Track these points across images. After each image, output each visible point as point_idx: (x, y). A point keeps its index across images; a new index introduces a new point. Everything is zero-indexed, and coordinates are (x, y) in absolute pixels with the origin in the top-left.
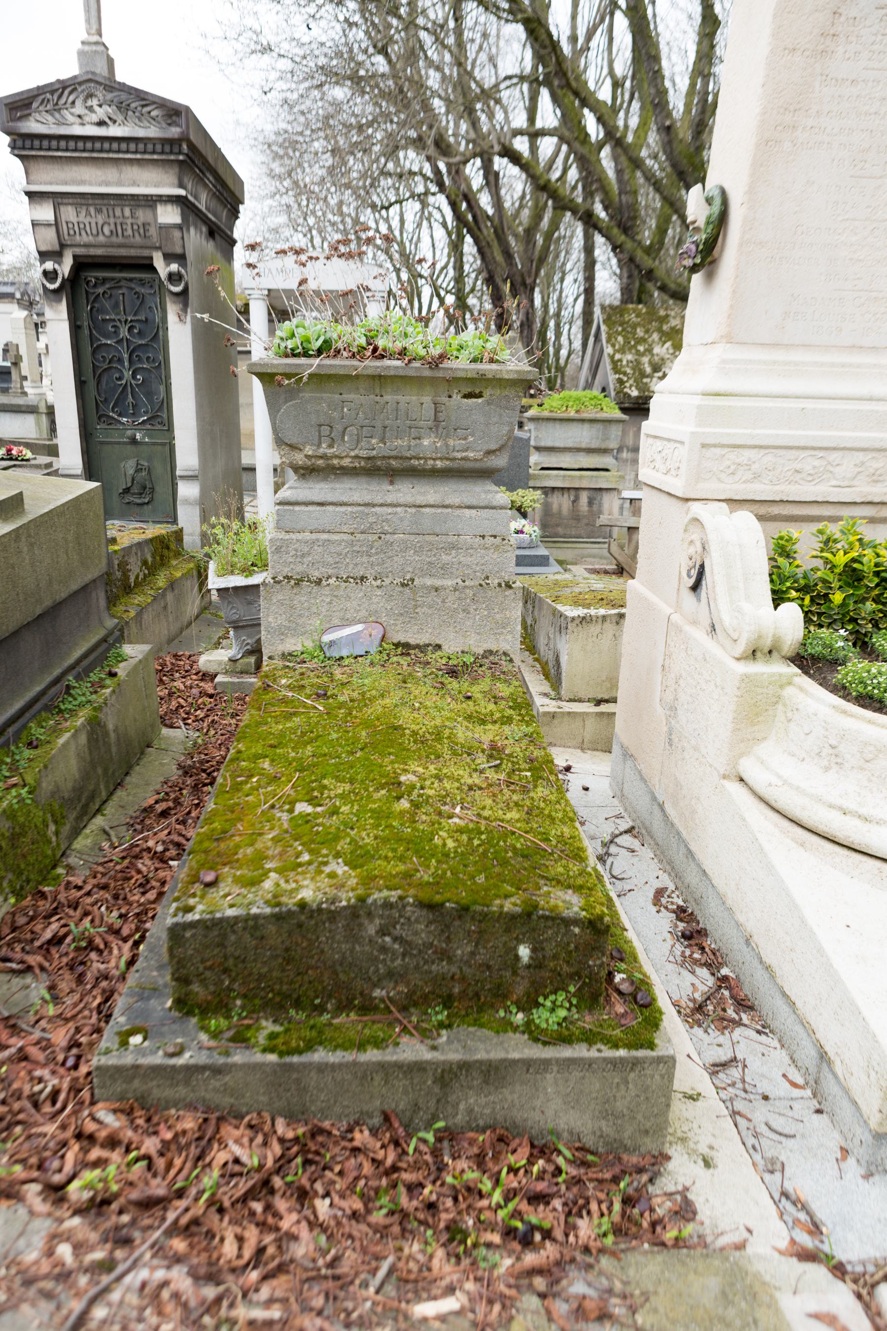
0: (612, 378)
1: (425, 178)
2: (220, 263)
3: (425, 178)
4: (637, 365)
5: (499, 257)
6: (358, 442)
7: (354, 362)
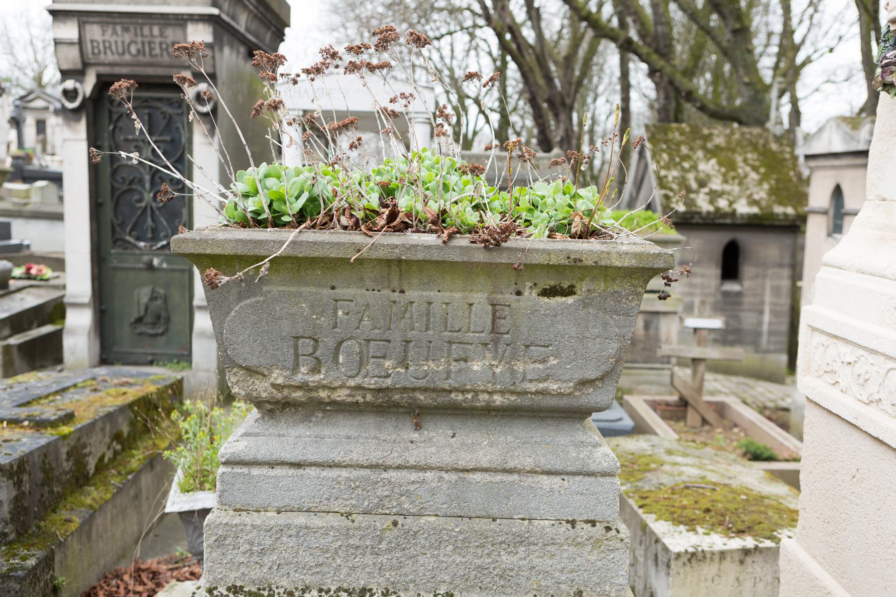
0: (657, 194)
1: (474, 13)
3: (474, 13)
4: (683, 183)
5: (541, 82)
6: (361, 364)
7: (356, 238)
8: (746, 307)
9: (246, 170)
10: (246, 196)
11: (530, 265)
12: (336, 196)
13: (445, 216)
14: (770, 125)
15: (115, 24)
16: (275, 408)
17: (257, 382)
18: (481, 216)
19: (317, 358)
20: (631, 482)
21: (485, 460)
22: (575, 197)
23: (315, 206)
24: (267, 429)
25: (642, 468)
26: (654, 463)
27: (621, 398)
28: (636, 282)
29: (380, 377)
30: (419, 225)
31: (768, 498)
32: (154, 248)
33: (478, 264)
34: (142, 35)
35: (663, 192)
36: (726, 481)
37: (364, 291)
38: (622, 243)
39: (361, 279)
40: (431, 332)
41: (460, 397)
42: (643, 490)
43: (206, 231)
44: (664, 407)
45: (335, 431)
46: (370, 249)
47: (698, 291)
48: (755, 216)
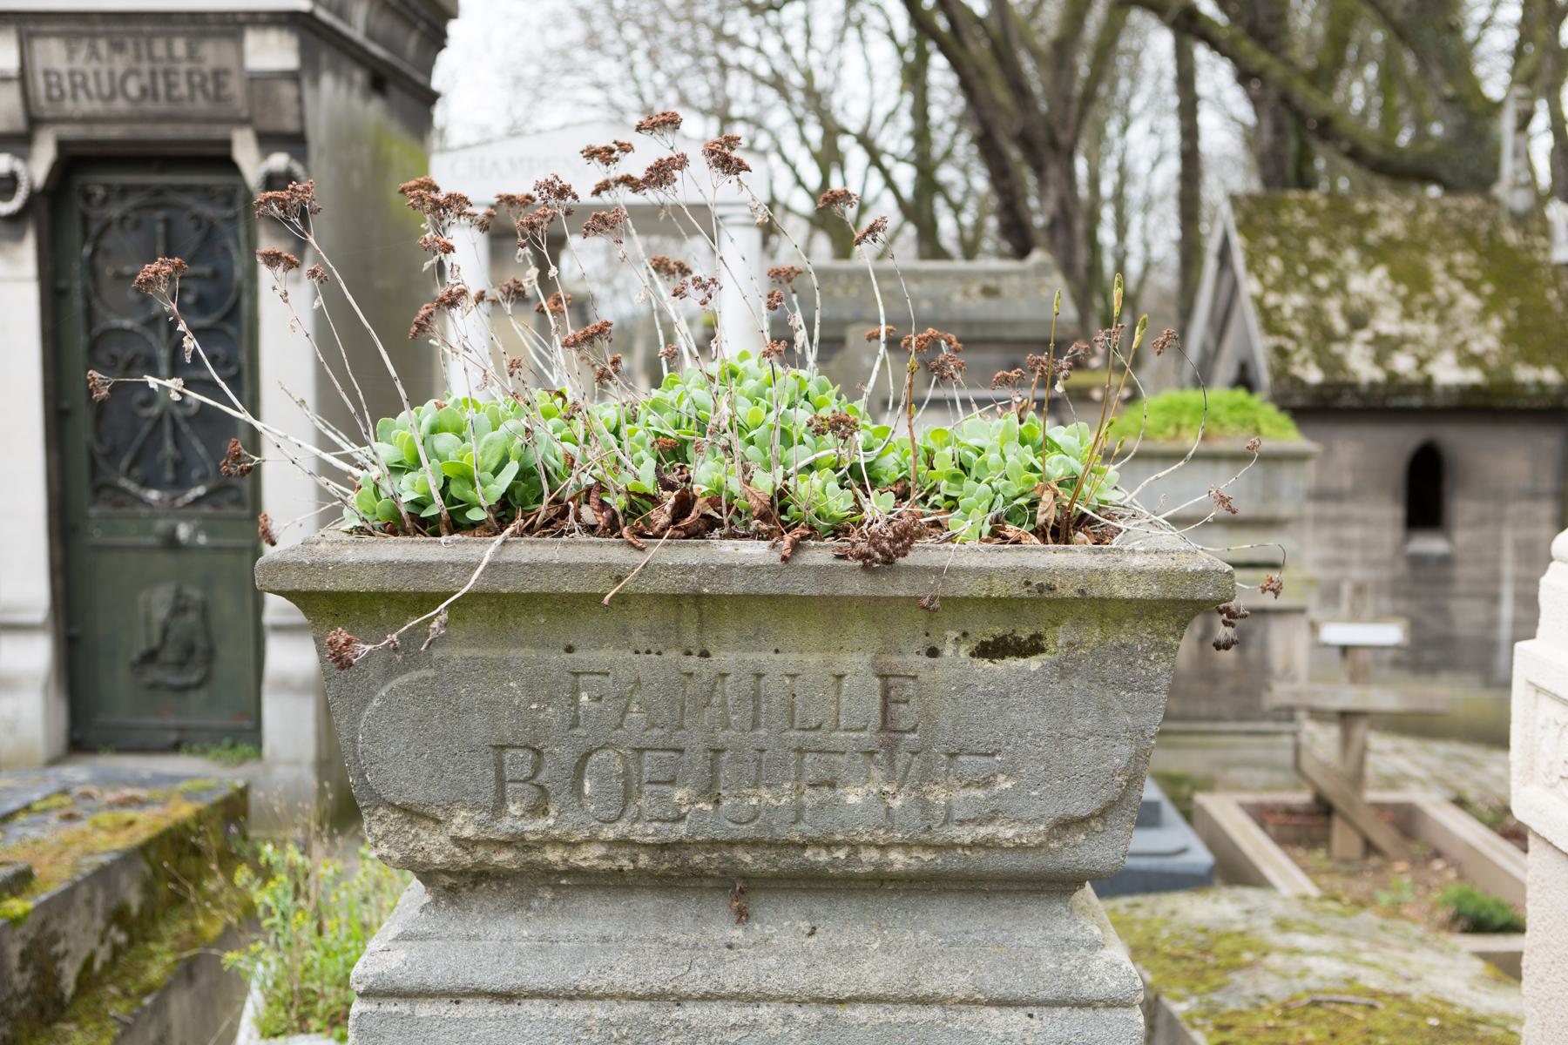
0: (1262, 346)
2: (398, 145)
5: (1003, 96)
6: (627, 796)
7: (614, 553)
8: (1461, 587)
9: (395, 416)
10: (397, 469)
11: (954, 598)
12: (572, 466)
13: (786, 500)
14: (1501, 190)
15: (94, 36)
16: (459, 883)
17: (424, 834)
18: (856, 499)
19: (540, 787)
20: (1200, 994)
21: (875, 980)
22: (1045, 447)
23: (531, 486)
24: (445, 926)
25: (1222, 962)
26: (1249, 949)
27: (1189, 799)
28: (1161, 626)
29: (664, 821)
30: (736, 520)
31: (1484, 1021)
32: (180, 503)
33: (851, 599)
34: (152, 58)
35: (1273, 341)
36: (1400, 988)
37: (630, 654)
38: (1133, 551)
39: (625, 631)
40: (762, 732)
41: (823, 857)
42: (1224, 1011)
43: (323, 546)
44: (1281, 818)
45: (577, 928)
46: (640, 574)
47: (1356, 555)
48: (1474, 389)
